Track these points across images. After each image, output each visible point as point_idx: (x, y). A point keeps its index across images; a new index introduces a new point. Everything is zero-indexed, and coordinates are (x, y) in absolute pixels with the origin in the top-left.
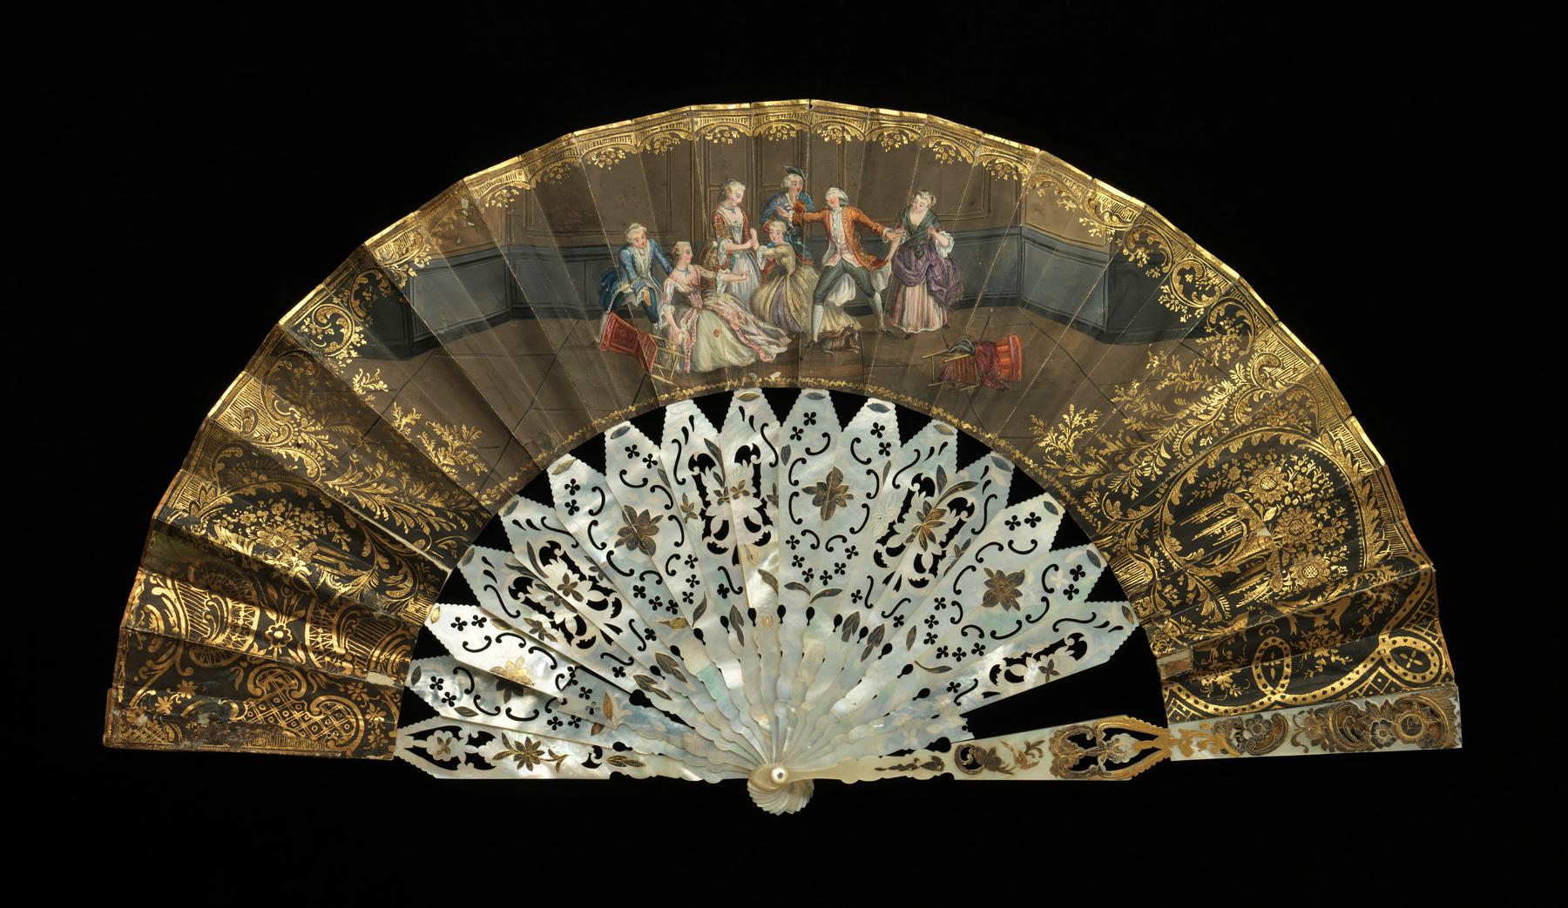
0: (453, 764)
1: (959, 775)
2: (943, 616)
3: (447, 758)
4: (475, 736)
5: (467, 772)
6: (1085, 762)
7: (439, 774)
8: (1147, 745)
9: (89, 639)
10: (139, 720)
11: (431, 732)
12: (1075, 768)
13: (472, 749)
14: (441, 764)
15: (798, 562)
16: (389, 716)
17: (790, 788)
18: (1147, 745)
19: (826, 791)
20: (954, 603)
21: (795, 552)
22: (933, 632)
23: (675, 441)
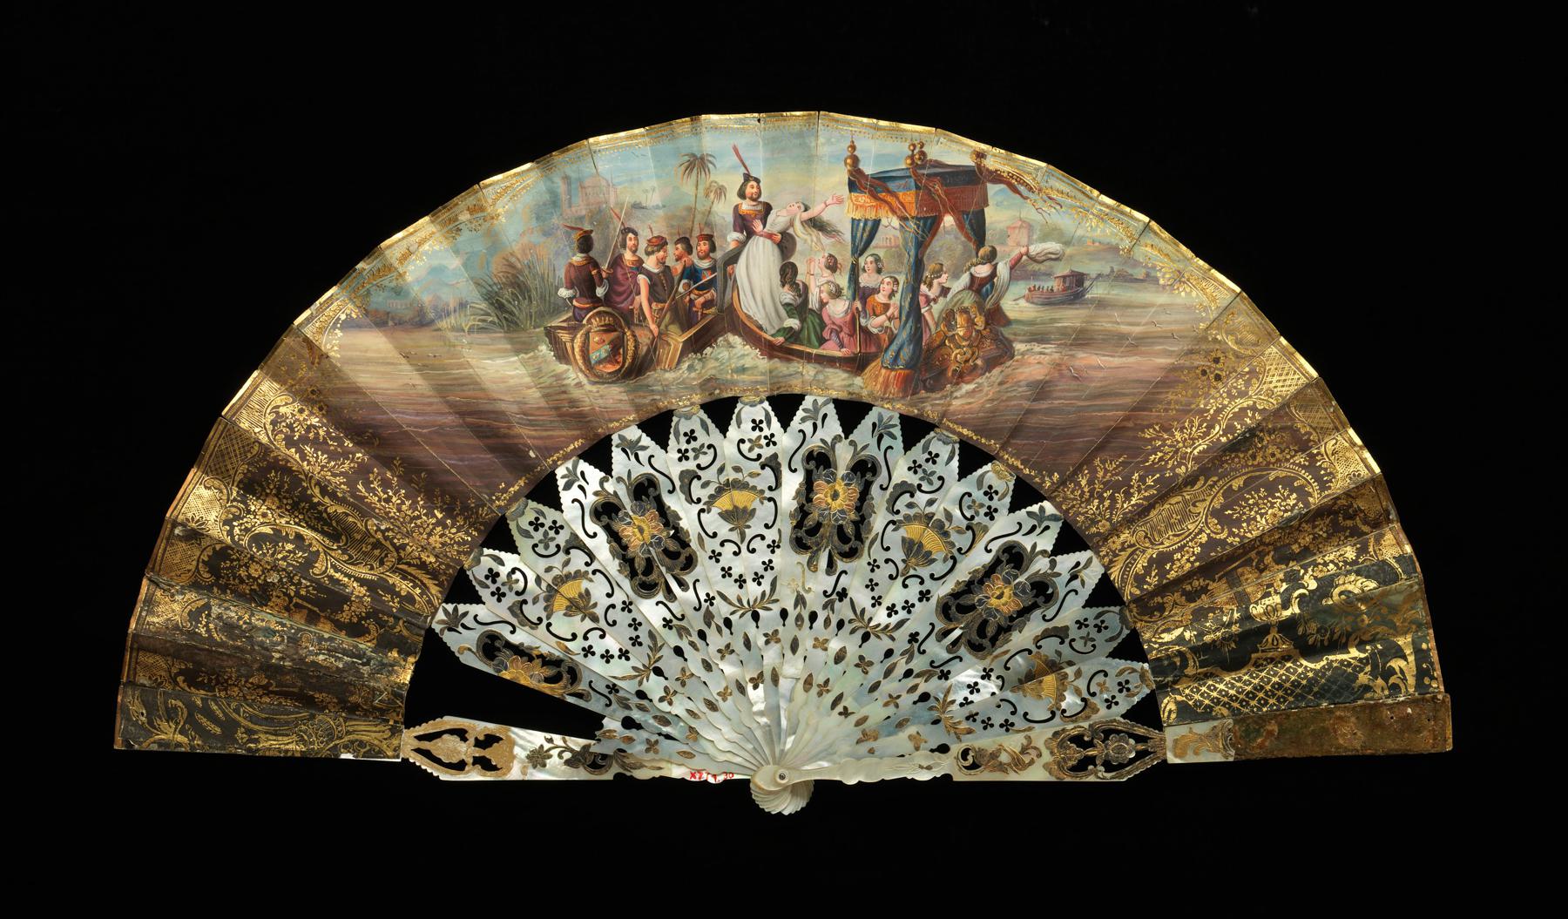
0: (460, 766)
1: (960, 777)
2: (599, 646)
3: (455, 761)
4: (481, 738)
5: (475, 775)
6: (1083, 765)
7: (445, 776)
8: (425, 745)
9: (97, 640)
10: (151, 723)
11: (438, 735)
12: (1074, 769)
13: (1091, 752)
14: (450, 766)
15: (872, 585)
16: (1074, 718)
17: (794, 789)
18: (425, 745)
19: (825, 792)
20: (585, 638)
21: (872, 576)
22: (617, 654)
23: (574, 500)
